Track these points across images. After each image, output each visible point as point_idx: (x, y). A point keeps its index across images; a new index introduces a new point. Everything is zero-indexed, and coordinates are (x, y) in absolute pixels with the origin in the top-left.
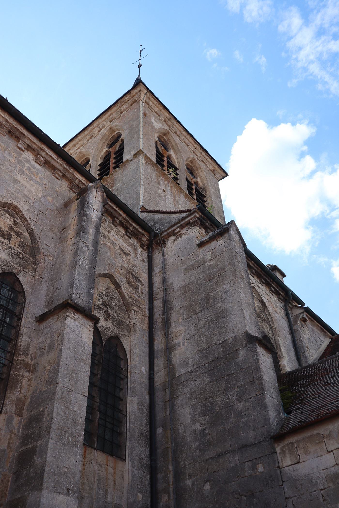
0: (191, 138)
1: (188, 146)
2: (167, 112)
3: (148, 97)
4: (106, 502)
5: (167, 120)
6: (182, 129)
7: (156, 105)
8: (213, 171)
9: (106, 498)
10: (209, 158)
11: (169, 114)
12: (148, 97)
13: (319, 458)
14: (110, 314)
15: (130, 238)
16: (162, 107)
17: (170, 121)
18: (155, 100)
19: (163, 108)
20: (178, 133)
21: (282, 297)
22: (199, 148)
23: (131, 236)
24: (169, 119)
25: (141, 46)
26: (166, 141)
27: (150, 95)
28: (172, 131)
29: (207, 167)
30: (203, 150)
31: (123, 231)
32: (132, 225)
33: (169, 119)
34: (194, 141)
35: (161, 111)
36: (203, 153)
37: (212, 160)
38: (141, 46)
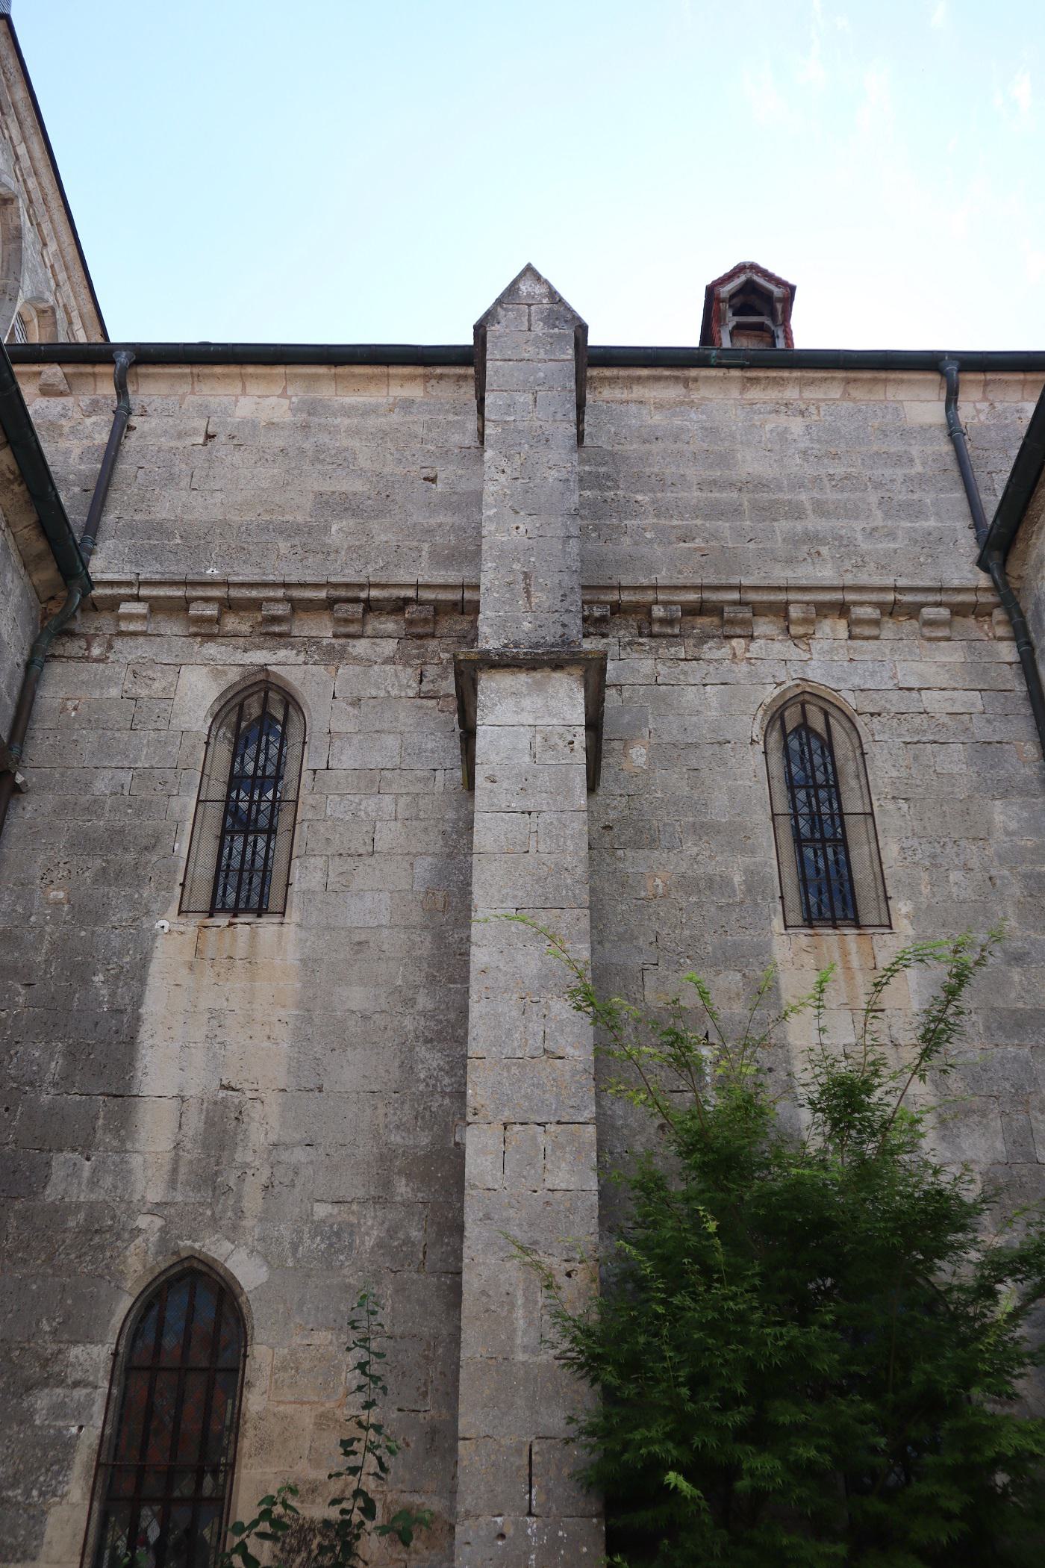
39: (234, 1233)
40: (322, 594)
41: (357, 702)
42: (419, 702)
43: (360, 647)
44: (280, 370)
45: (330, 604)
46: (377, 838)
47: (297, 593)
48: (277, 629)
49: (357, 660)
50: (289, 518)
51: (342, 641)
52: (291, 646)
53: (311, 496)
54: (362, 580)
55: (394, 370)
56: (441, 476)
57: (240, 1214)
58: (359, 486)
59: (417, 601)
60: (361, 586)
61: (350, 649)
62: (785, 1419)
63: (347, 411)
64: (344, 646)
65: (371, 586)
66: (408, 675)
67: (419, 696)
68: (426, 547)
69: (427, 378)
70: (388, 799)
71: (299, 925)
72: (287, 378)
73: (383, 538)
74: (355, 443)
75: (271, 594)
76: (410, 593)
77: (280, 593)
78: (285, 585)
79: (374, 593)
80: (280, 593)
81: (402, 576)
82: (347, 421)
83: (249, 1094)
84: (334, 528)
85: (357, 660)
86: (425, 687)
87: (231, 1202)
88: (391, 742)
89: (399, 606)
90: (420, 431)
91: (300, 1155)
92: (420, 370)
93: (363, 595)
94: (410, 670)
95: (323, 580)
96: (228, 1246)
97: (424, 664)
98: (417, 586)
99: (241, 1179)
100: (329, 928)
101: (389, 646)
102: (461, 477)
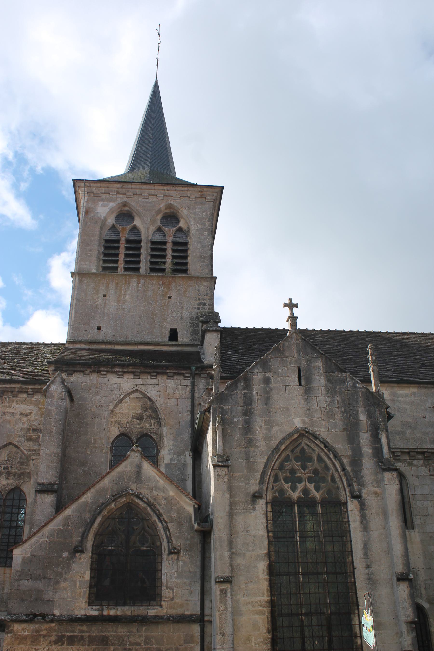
0: (156, 185)
1: (156, 195)
2: (115, 184)
3: (89, 186)
4: (3, 594)
5: (120, 190)
6: (140, 186)
7: (100, 187)
8: (202, 197)
9: (3, 591)
10: (190, 187)
11: (118, 184)
12: (89, 186)
13: (266, 525)
14: (11, 473)
15: (33, 397)
16: (107, 183)
17: (124, 188)
18: (97, 183)
19: (109, 183)
20: (138, 191)
21: (187, 375)
22: (172, 187)
23: (32, 396)
24: (122, 187)
25: (159, 25)
26: (129, 211)
27: (89, 183)
28: (130, 196)
29: (191, 199)
30: (177, 186)
31: (25, 396)
32: (28, 389)
33: (122, 187)
34: (161, 186)
35: (108, 187)
36: (179, 187)
37: (194, 187)
38: (159, 25)
39: (421, 597)
40: (408, 450)
41: (417, 477)
42: (431, 477)
43: (415, 462)
44: (386, 385)
45: (408, 453)
46: (429, 511)
47: (402, 450)
48: (398, 458)
49: (415, 466)
50: (396, 429)
51: (411, 461)
52: (400, 462)
53: (400, 422)
54: (416, 447)
55: (412, 385)
56: (427, 416)
57: (421, 594)
58: (409, 420)
59: (427, 452)
60: (416, 449)
61: (413, 463)
62: (165, 611)
63: (402, 396)
64: (412, 462)
65: (418, 448)
66: (427, 470)
67: (430, 475)
68: (428, 438)
69: (419, 387)
70: (429, 502)
71: (418, 532)
72: (388, 386)
73: (418, 435)
74: (405, 406)
75: (397, 450)
76: (426, 450)
77: (399, 450)
78: (400, 448)
79: (419, 450)
80: (399, 450)
81: (425, 446)
82: (402, 399)
83: (417, 570)
84: (407, 432)
85: (415, 466)
86: (431, 473)
87: (419, 592)
88: (426, 487)
89: (423, 453)
90: (419, 402)
91: (429, 582)
92: (418, 385)
93: (416, 450)
94: (427, 469)
95: (408, 447)
96: (421, 601)
97: (429, 467)
98: (427, 449)
99: (420, 587)
100: (424, 533)
101: (421, 462)
102: (431, 417)
